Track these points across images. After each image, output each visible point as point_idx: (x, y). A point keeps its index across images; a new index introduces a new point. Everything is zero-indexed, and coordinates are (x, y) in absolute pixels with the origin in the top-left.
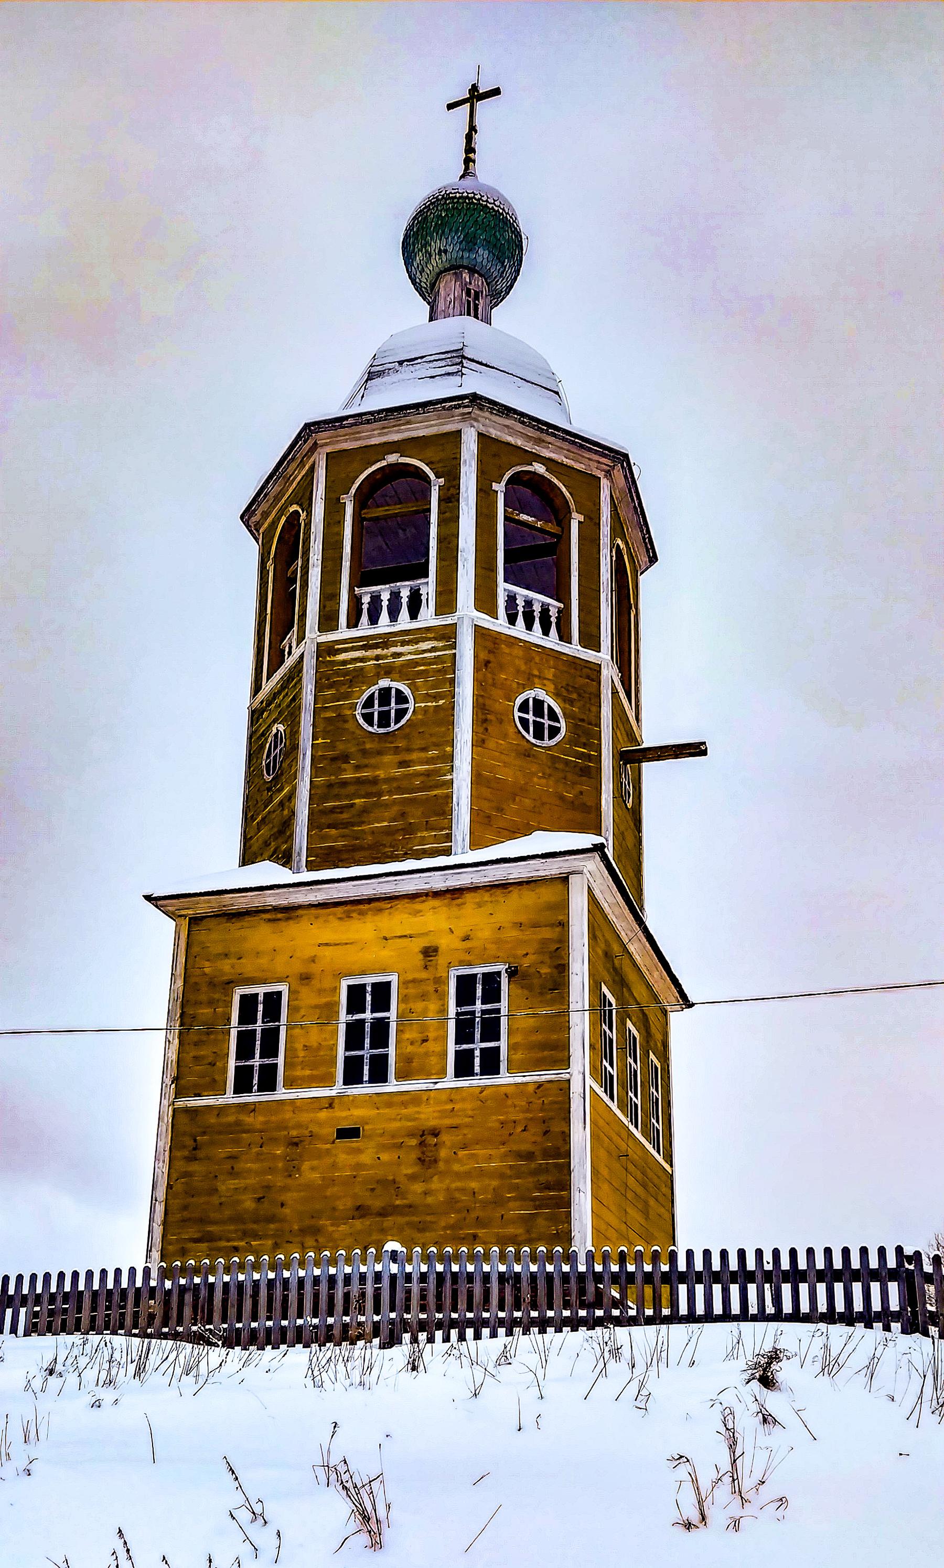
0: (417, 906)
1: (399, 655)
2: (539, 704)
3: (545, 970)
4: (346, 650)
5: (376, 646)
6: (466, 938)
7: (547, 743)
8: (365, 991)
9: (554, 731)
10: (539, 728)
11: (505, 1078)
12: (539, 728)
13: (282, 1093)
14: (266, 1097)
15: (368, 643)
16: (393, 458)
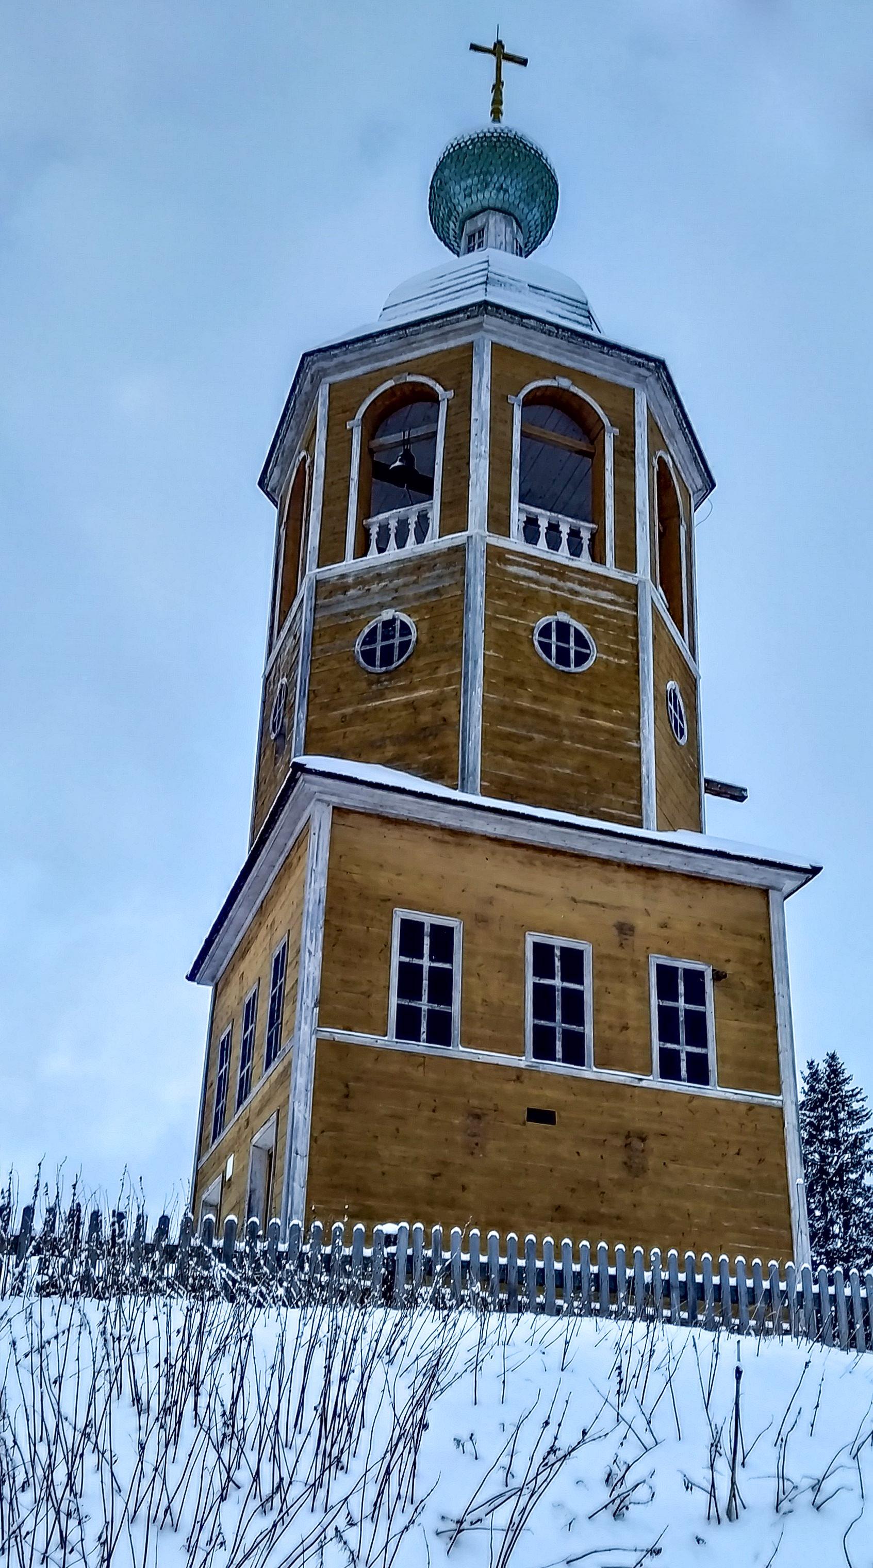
0: (583, 863)
1: (577, 593)
2: (563, 628)
3: (749, 983)
4: (518, 564)
5: (551, 573)
6: (664, 926)
7: (572, 668)
9: (581, 658)
11: (714, 1091)
13: (459, 1051)
14: (438, 1050)
15: (544, 567)
16: (564, 383)
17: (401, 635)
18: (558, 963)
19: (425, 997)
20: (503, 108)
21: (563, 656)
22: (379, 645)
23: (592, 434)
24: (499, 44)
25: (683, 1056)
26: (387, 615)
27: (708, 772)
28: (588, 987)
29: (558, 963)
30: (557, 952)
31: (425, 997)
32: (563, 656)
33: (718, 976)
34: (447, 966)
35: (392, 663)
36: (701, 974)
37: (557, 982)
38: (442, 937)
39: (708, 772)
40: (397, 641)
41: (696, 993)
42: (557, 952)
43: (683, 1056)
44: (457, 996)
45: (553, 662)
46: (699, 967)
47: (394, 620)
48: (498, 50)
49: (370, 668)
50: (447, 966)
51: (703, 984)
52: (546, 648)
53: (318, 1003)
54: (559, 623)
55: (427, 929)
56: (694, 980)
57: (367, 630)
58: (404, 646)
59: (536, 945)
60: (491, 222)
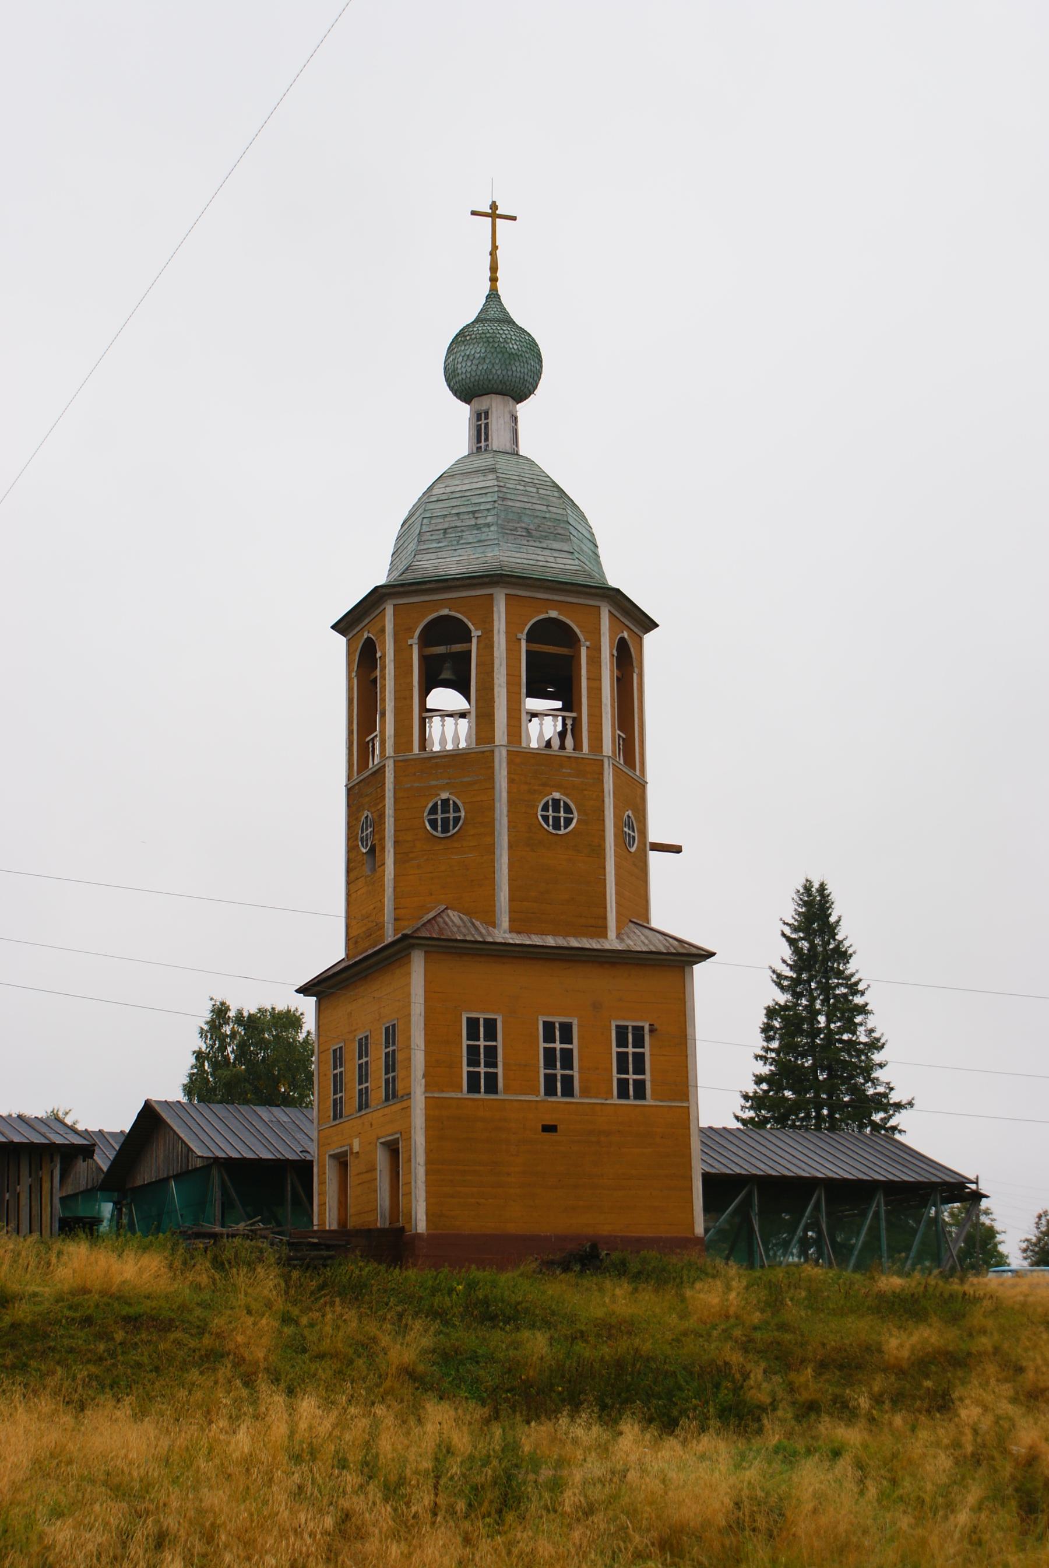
2: (556, 802)
8: (682, 1100)
9: (568, 821)
10: (557, 820)
12: (557, 820)
17: (454, 811)
18: (557, 1033)
19: (482, 1039)
20: (499, 274)
21: (556, 826)
22: (439, 816)
23: (575, 636)
24: (494, 206)
25: (631, 1082)
26: (444, 796)
27: (653, 837)
28: (575, 1046)
29: (557, 1033)
30: (557, 1025)
31: (482, 1039)
32: (556, 826)
33: (652, 1031)
34: (494, 1043)
35: (449, 831)
36: (642, 1028)
37: (558, 1045)
38: (491, 1025)
39: (653, 837)
40: (452, 815)
41: (639, 1042)
42: (557, 1025)
43: (631, 1082)
44: (500, 1064)
45: (550, 829)
46: (640, 1024)
47: (448, 800)
48: (493, 214)
49: (435, 833)
50: (494, 1043)
51: (643, 1036)
52: (546, 819)
53: (425, 1076)
54: (553, 800)
55: (482, 1022)
56: (638, 1031)
57: (430, 805)
58: (457, 820)
59: (544, 1022)
60: (494, 405)
